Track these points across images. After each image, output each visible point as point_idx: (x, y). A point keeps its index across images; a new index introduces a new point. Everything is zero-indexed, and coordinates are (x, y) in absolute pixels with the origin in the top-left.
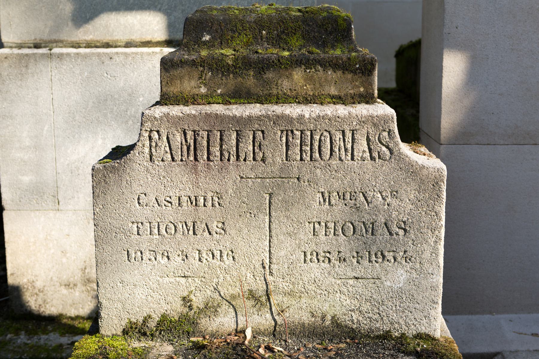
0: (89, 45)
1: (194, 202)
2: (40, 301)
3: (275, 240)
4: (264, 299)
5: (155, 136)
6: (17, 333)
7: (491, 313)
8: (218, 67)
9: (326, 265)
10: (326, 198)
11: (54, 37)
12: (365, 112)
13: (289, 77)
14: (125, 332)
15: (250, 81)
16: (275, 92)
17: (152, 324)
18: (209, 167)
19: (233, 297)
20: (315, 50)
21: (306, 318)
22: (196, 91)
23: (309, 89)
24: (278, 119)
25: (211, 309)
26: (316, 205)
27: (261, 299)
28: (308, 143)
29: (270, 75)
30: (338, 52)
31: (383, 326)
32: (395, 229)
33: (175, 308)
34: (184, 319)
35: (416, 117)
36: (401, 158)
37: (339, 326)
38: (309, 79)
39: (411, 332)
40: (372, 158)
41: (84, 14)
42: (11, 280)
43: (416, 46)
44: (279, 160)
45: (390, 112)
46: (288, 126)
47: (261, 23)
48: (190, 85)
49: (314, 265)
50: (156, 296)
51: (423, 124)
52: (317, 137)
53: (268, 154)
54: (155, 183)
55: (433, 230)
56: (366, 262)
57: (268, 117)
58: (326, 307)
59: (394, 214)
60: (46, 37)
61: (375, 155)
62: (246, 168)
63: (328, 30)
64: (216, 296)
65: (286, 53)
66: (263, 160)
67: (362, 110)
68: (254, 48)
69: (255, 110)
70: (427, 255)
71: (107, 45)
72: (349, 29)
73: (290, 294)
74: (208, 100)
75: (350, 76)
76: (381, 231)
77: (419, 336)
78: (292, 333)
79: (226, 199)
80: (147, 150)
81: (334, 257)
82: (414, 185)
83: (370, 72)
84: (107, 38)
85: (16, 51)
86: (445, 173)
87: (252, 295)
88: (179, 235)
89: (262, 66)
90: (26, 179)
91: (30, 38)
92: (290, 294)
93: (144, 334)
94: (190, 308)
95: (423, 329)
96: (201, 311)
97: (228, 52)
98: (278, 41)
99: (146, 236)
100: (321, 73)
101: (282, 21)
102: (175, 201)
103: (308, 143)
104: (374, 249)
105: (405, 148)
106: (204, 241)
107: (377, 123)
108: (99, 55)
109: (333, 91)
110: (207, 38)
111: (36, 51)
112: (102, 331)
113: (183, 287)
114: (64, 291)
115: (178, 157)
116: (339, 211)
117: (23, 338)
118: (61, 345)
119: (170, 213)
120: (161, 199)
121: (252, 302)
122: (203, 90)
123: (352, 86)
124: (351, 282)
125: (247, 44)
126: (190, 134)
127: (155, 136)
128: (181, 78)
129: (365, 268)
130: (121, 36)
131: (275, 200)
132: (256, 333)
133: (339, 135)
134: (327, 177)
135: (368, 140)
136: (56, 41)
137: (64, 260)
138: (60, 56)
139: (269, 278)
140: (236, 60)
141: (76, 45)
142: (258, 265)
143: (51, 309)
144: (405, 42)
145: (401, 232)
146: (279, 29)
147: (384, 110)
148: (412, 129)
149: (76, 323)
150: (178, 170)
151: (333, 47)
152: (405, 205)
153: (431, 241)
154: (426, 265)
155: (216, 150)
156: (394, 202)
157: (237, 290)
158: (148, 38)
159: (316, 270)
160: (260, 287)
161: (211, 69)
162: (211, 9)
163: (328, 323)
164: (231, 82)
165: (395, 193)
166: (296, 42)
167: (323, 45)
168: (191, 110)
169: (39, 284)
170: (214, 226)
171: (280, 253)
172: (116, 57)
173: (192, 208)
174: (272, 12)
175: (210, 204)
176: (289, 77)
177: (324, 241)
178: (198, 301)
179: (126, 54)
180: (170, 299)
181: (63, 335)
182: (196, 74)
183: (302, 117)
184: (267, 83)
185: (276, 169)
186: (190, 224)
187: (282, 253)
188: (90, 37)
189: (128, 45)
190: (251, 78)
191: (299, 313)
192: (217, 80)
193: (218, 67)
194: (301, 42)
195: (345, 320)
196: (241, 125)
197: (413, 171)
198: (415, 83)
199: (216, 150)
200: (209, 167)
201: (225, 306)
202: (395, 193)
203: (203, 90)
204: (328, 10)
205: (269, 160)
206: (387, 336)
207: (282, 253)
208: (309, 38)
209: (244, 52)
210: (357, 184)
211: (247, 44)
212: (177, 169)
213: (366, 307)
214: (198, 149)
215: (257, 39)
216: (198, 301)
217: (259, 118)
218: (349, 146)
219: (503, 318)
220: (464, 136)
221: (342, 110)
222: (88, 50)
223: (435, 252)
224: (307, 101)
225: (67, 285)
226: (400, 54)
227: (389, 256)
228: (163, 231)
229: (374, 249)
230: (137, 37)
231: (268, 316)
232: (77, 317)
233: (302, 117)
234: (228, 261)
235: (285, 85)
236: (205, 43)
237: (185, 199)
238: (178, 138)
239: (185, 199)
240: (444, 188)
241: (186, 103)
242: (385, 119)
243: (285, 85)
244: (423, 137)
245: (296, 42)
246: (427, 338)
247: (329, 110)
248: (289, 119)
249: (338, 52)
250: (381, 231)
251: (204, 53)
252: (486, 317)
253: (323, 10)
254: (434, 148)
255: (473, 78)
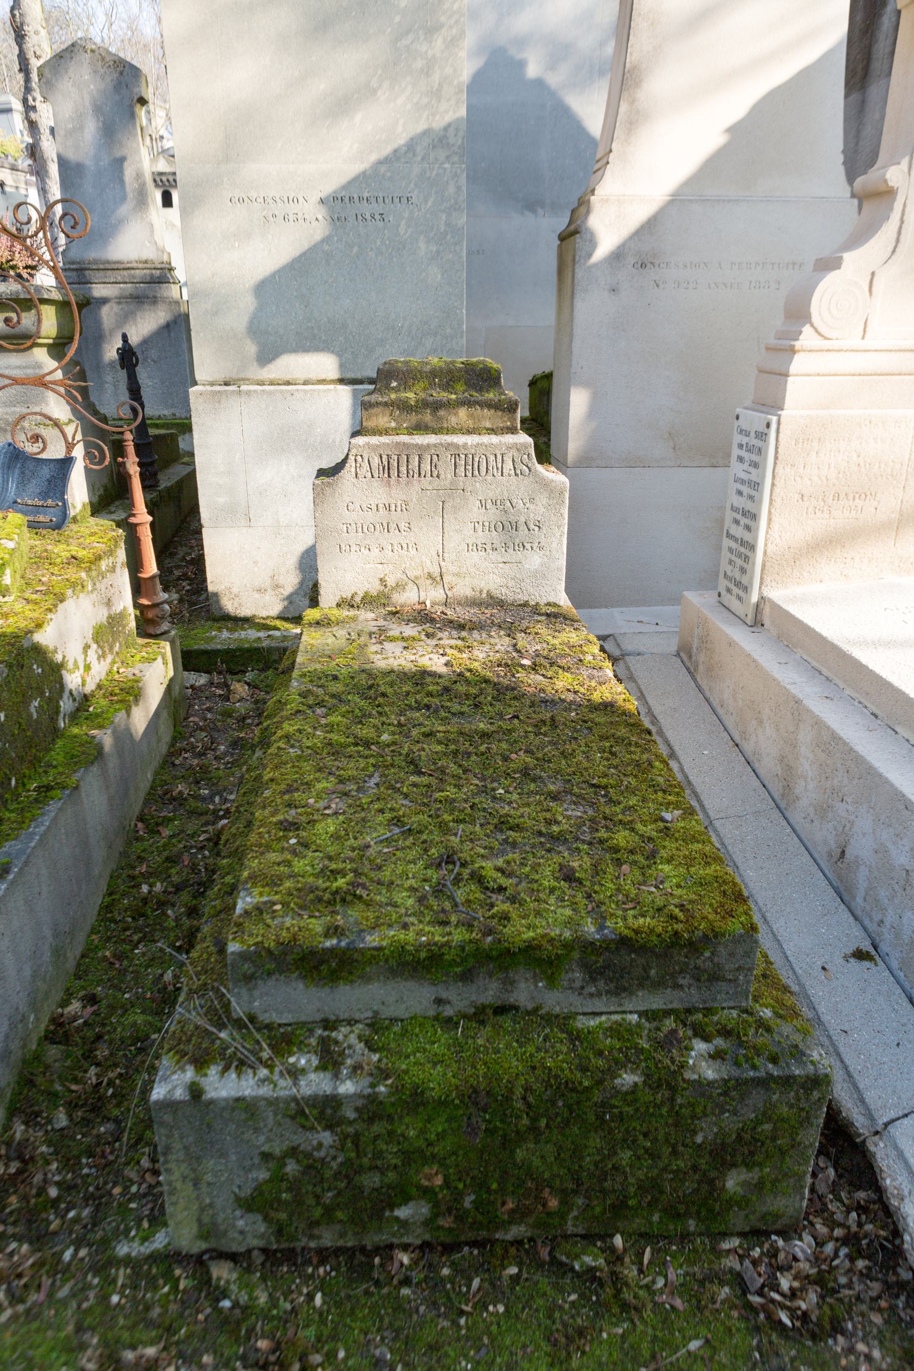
0: (272, 383)
1: (388, 508)
2: (236, 605)
3: (446, 535)
4: (438, 579)
5: (359, 459)
6: (219, 629)
7: (606, 607)
8: (404, 407)
9: (483, 553)
10: (483, 505)
11: (241, 376)
12: (511, 441)
13: (456, 414)
14: (338, 605)
15: (427, 417)
16: (445, 425)
17: (358, 599)
18: (398, 482)
19: (417, 578)
20: (475, 394)
21: (469, 593)
22: (388, 425)
23: (470, 424)
24: (448, 446)
25: (400, 587)
26: (476, 509)
27: (437, 579)
28: (470, 464)
29: (442, 413)
30: (491, 395)
31: (522, 598)
32: (532, 526)
33: (374, 588)
34: (381, 595)
35: (548, 444)
36: (536, 474)
37: (492, 597)
38: (471, 416)
39: (543, 602)
40: (516, 475)
41: (266, 357)
42: (211, 588)
43: (548, 377)
44: (449, 476)
45: (530, 440)
46: (456, 452)
47: (434, 373)
48: (383, 420)
49: (474, 553)
50: (360, 577)
51: (554, 451)
52: (476, 459)
53: (442, 472)
54: (358, 491)
55: (559, 527)
56: (511, 551)
57: (441, 444)
58: (483, 585)
59: (532, 515)
60: (234, 376)
61: (518, 472)
62: (426, 482)
63: (481, 379)
64: (404, 577)
65: (453, 397)
66: (438, 477)
67: (509, 439)
68: (429, 392)
69: (431, 439)
70: (554, 545)
71: (288, 383)
72: (499, 378)
73: (457, 575)
74: (396, 431)
75: (500, 413)
76: (522, 527)
77: (549, 604)
78: (459, 604)
79: (410, 508)
80: (353, 470)
81: (488, 547)
82: (546, 494)
83: (515, 411)
84: (288, 377)
85: (209, 388)
86: (568, 485)
87: (430, 576)
88: (377, 533)
89: (437, 406)
90: (221, 500)
91: (220, 376)
92: (457, 575)
93: (353, 606)
94: (385, 586)
95: (552, 599)
96: (393, 589)
97: (411, 395)
98: (447, 386)
99: (352, 534)
100: (479, 411)
101: (450, 371)
102: (374, 508)
103: (470, 464)
104: (517, 541)
105: (540, 468)
106: (394, 535)
107: (519, 448)
108: (281, 391)
109: (488, 425)
110: (394, 384)
111: (226, 388)
112: (321, 604)
113: (381, 571)
114: (257, 596)
115: (376, 475)
116: (493, 514)
117: (225, 634)
118: (259, 638)
119: (370, 517)
120: (364, 506)
121: (430, 581)
122: (393, 424)
123: (500, 420)
124: (501, 565)
125: (425, 389)
126: (385, 458)
127: (359, 459)
128: (377, 415)
129: (512, 555)
130: (301, 376)
131: (446, 505)
132: (434, 604)
133: (492, 458)
134: (485, 487)
135: (513, 461)
136: (243, 380)
137: (256, 569)
138: (248, 393)
139: (442, 564)
140: (417, 402)
141: (261, 383)
142: (434, 554)
143: (245, 612)
144: (538, 372)
145: (536, 529)
146: (447, 377)
147: (524, 439)
148: (544, 455)
149: (268, 622)
150: (376, 484)
151: (488, 391)
152: (538, 510)
153: (558, 535)
154: (554, 553)
155: (403, 469)
156: (532, 507)
157: (418, 573)
158: (323, 377)
159: (476, 557)
160: (436, 571)
161: (398, 408)
162: (397, 362)
163: (484, 595)
164: (414, 418)
165: (532, 500)
166: (460, 387)
167: (480, 390)
168: (385, 439)
169: (235, 590)
170: (402, 526)
171: (450, 545)
172: (296, 394)
173: (386, 513)
174: (442, 364)
175: (399, 509)
176: (456, 414)
177: (482, 536)
178: (391, 582)
179: (305, 391)
180: (371, 580)
181: (259, 630)
182: (388, 413)
183: (466, 444)
184: (440, 419)
185: (447, 483)
186: (385, 525)
187: (452, 545)
188: (272, 376)
189: (305, 383)
190: (426, 415)
191: (464, 589)
192: (404, 417)
193: (404, 407)
194: (464, 387)
195: (496, 593)
196: (422, 450)
197: (545, 485)
198: (548, 413)
199: (403, 469)
200: (398, 482)
201: (411, 584)
202: (532, 500)
203: (393, 424)
204: (483, 362)
205: (442, 476)
206: (525, 605)
207: (452, 545)
208: (470, 385)
209: (422, 395)
210: (506, 493)
211: (425, 389)
212: (375, 483)
213: (511, 583)
214: (389, 468)
215: (432, 385)
216: (391, 582)
217: (435, 445)
218: (500, 466)
219: (616, 611)
220: (586, 461)
221: (494, 439)
222: (272, 388)
223: (560, 543)
224: (469, 432)
225: (259, 591)
226: (533, 384)
227: (528, 546)
228: (365, 530)
229: (517, 541)
230: (313, 376)
231: (442, 591)
232: (268, 617)
233: (466, 444)
234: (413, 552)
235: (453, 420)
236: (393, 388)
237: (381, 506)
238: (376, 461)
239: (381, 506)
240: (567, 495)
241: (381, 434)
242: (525, 446)
243: (453, 420)
244: (552, 461)
245: (460, 387)
246: (555, 605)
247: (486, 439)
248: (457, 447)
249: (491, 395)
250: (522, 527)
251: (393, 396)
252: (603, 611)
253: (479, 362)
254: (562, 466)
255: (593, 412)
